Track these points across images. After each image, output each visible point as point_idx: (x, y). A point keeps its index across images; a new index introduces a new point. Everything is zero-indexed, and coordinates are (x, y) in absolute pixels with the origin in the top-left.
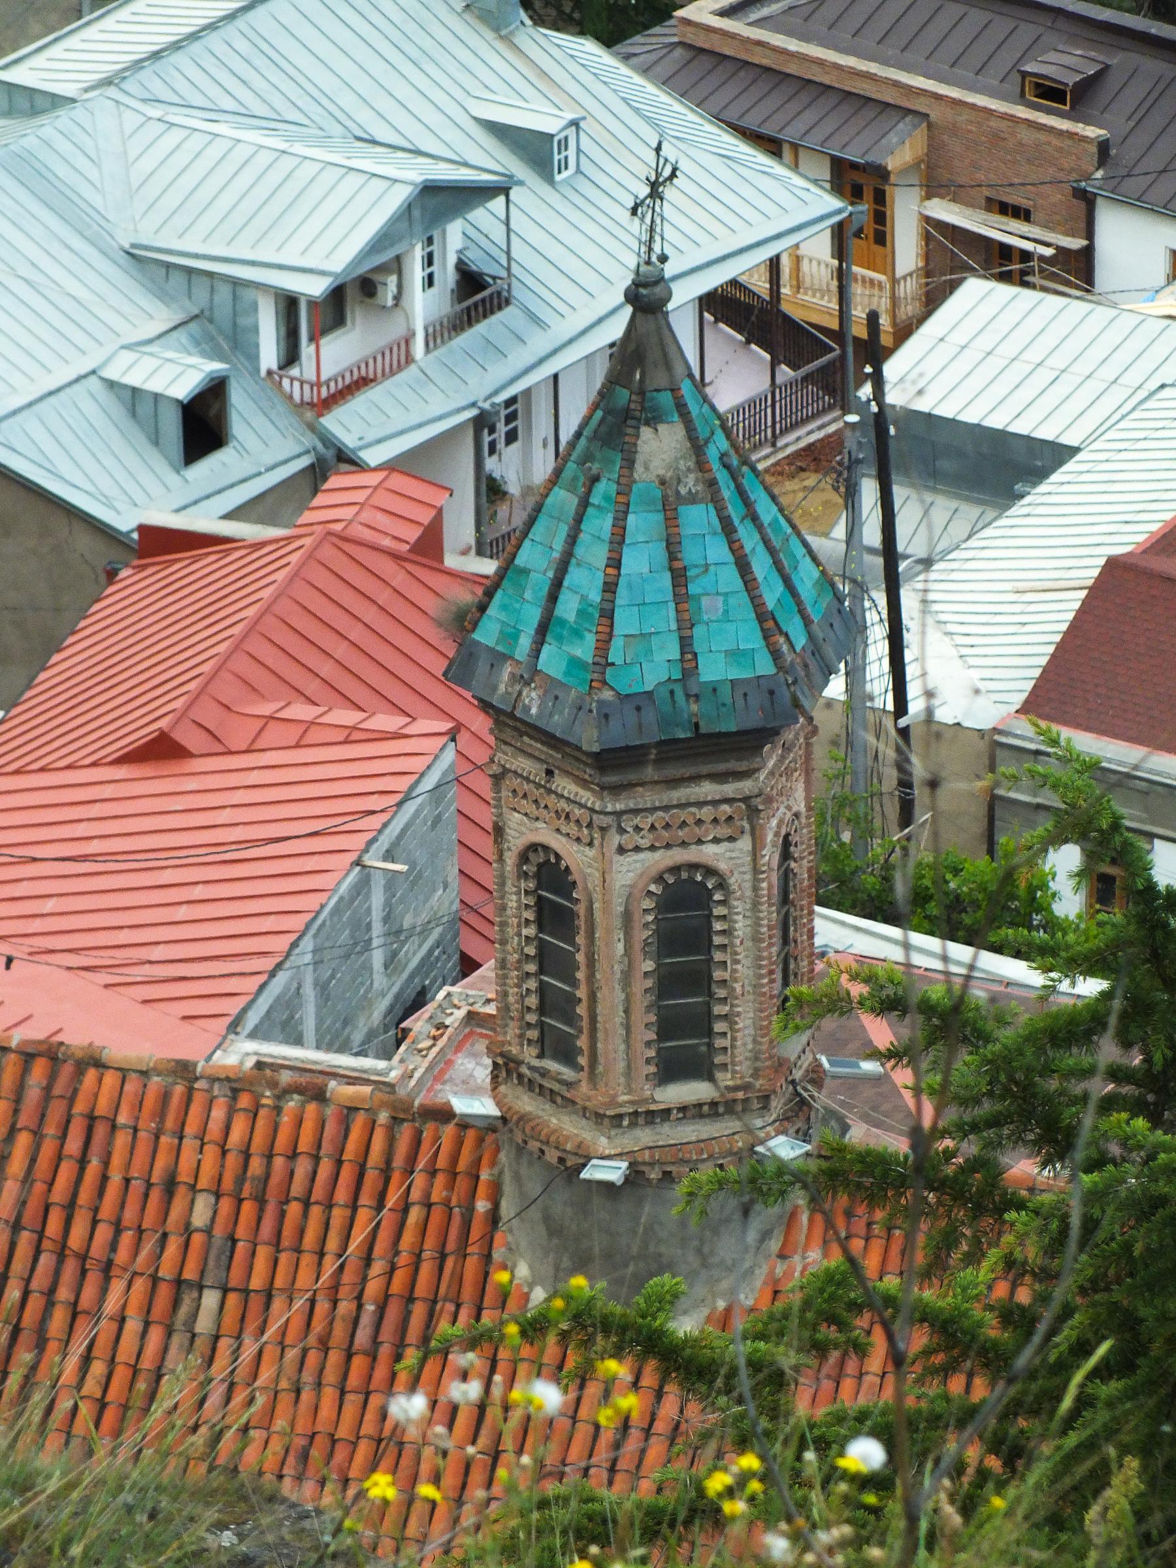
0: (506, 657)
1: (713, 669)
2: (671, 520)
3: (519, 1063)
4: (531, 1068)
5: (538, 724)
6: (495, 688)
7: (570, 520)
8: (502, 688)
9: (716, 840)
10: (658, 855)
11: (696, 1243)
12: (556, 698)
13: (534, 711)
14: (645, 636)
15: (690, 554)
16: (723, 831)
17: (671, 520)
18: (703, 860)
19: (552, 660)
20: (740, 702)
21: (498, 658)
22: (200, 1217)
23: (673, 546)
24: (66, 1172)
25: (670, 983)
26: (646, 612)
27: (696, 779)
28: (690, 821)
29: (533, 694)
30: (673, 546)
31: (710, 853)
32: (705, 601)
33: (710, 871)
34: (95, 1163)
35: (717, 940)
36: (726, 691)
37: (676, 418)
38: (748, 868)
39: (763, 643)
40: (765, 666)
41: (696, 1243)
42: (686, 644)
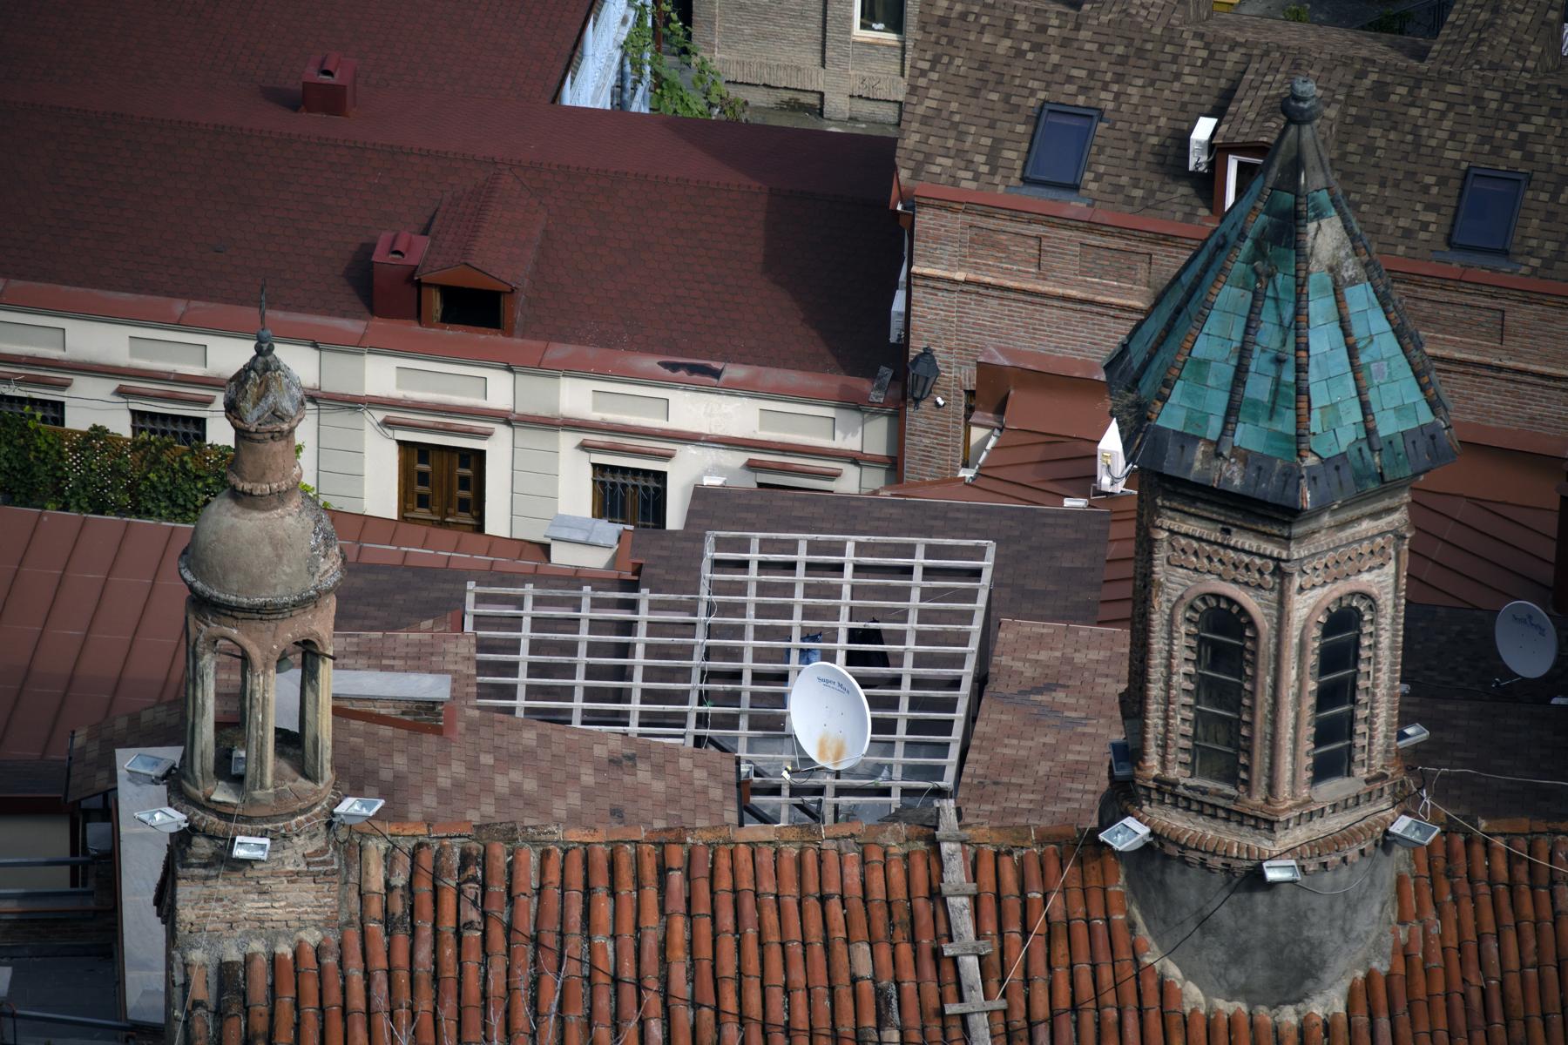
0: (1196, 439)
1: (1387, 426)
2: (1340, 302)
3: (1174, 784)
4: (1186, 787)
5: (1245, 492)
6: (1190, 466)
7: (1353, 318)
8: (1197, 465)
9: (1371, 569)
10: (1326, 589)
11: (1340, 922)
12: (1260, 468)
13: (1237, 482)
14: (1334, 406)
15: (1358, 330)
16: (1377, 561)
17: (1340, 302)
18: (1354, 588)
19: (1247, 435)
20: (1410, 447)
21: (1186, 440)
22: (864, 968)
23: (1344, 325)
24: (727, 944)
25: (1326, 697)
26: (1329, 387)
27: (1359, 519)
28: (1353, 556)
29: (1235, 468)
30: (1344, 325)
31: (1366, 580)
32: (1373, 367)
33: (1365, 596)
34: (751, 932)
35: (1364, 654)
36: (1399, 440)
37: (1333, 212)
38: (1391, 589)
39: (1421, 396)
40: (1426, 416)
41: (1340, 922)
42: (1365, 407)
